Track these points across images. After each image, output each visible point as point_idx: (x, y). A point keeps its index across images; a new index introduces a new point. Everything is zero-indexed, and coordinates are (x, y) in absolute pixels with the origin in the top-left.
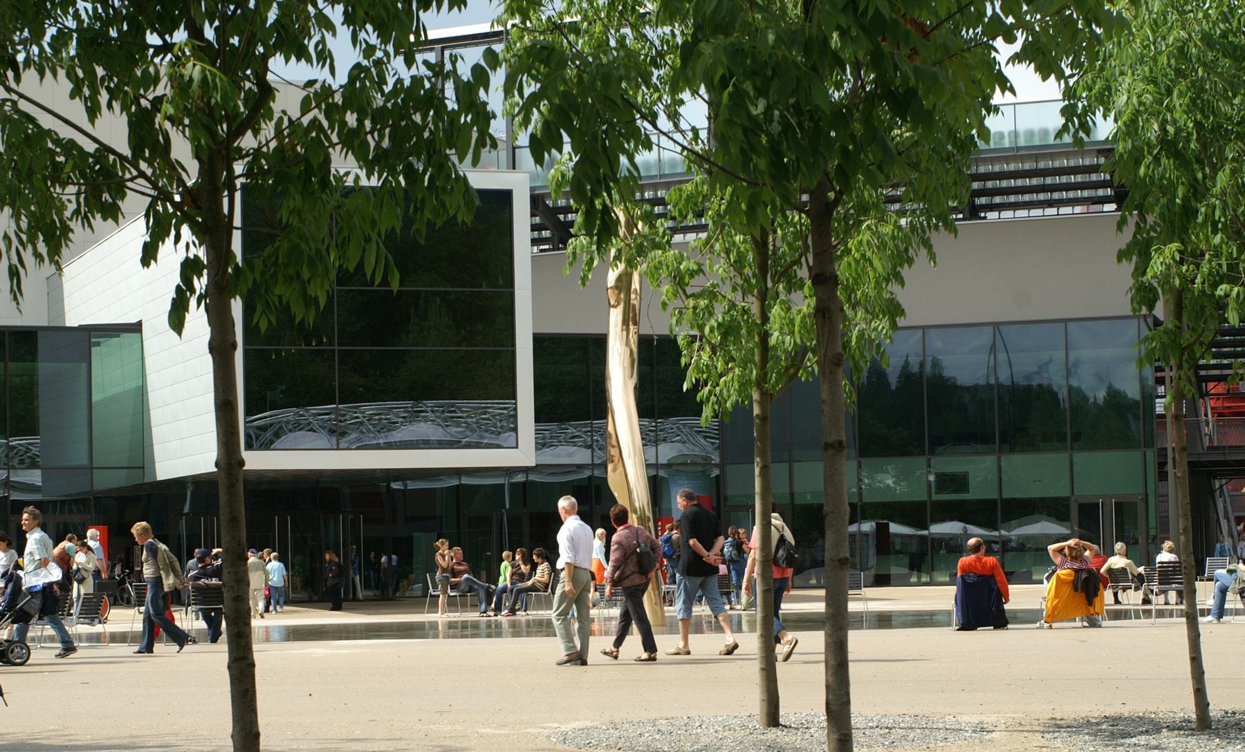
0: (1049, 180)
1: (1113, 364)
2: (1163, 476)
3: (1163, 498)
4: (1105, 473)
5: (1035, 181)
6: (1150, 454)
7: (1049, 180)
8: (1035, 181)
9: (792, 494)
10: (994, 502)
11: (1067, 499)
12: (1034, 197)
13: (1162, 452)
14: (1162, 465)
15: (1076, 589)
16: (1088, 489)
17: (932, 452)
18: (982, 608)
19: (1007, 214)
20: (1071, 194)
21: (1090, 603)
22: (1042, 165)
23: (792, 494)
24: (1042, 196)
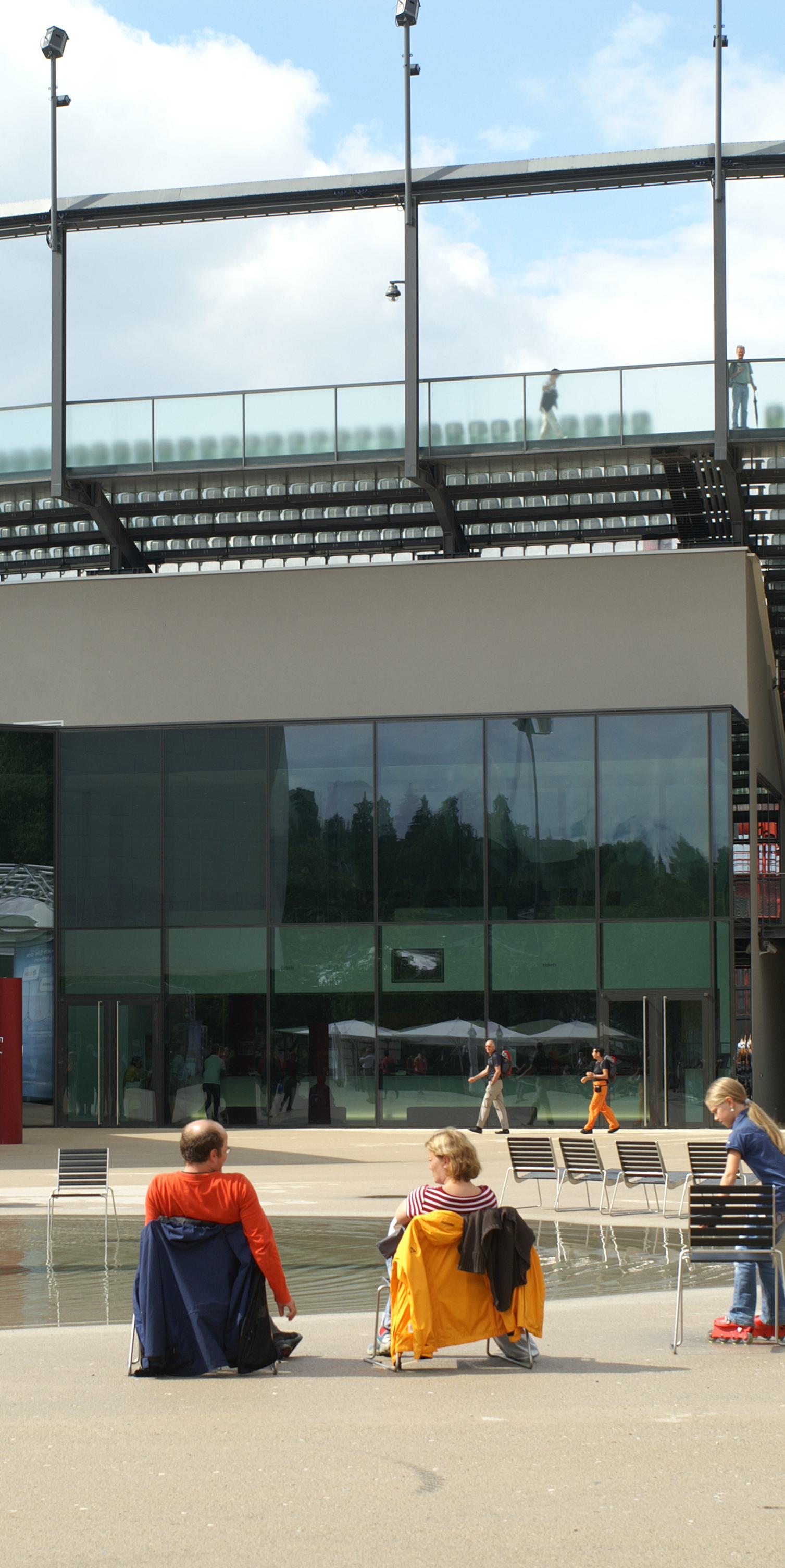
0: (577, 499)
1: (673, 798)
2: (742, 960)
3: (741, 992)
4: (655, 956)
5: (556, 501)
6: (724, 928)
7: (577, 499)
8: (556, 501)
9: (165, 978)
10: (367, 997)
11: (593, 994)
12: (556, 525)
13: (743, 926)
14: (742, 944)
15: (465, 1264)
16: (619, 981)
17: (387, 915)
18: (212, 1303)
19: (514, 552)
20: (612, 523)
21: (503, 1301)
22: (567, 474)
23: (165, 978)
24: (566, 525)
